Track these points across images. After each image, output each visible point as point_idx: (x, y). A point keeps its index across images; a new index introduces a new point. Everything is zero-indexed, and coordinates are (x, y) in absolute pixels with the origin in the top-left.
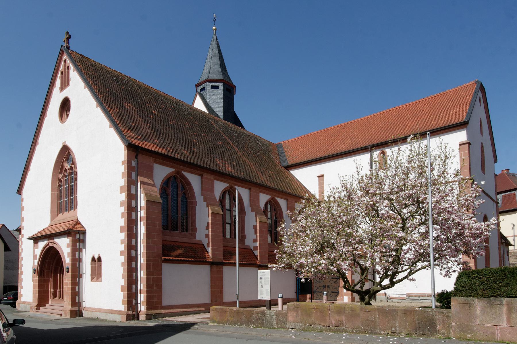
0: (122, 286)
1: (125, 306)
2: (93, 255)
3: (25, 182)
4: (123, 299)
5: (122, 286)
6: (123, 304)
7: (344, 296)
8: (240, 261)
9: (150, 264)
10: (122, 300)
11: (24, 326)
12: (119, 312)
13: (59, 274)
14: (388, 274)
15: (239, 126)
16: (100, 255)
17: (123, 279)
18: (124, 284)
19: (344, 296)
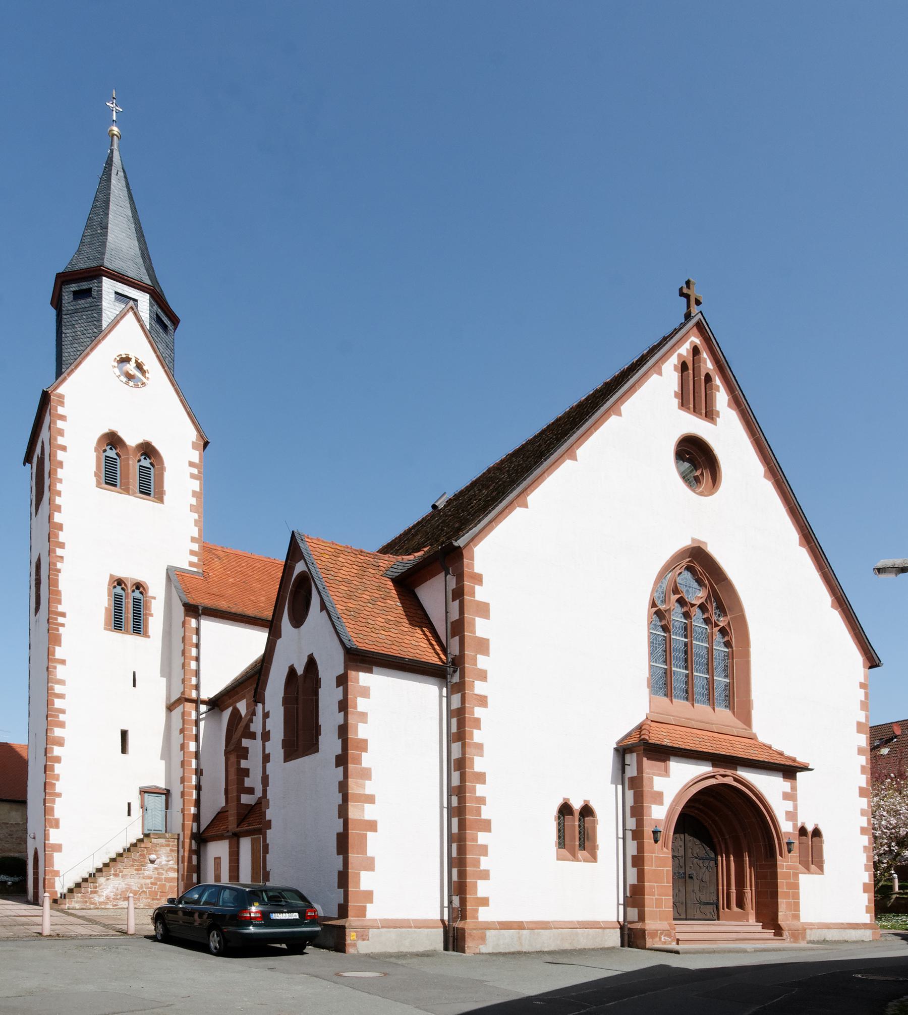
0: (865, 884)
1: (871, 916)
2: (815, 825)
3: (750, 439)
4: (867, 904)
5: (865, 884)
6: (867, 912)
7: (342, 767)
8: (901, 882)
9: (765, 862)
10: (866, 906)
11: (46, 415)
12: (865, 926)
13: (725, 855)
14: (888, 906)
15: (711, 849)
16: (817, 825)
17: (867, 873)
18: (870, 881)
19: (342, 767)
